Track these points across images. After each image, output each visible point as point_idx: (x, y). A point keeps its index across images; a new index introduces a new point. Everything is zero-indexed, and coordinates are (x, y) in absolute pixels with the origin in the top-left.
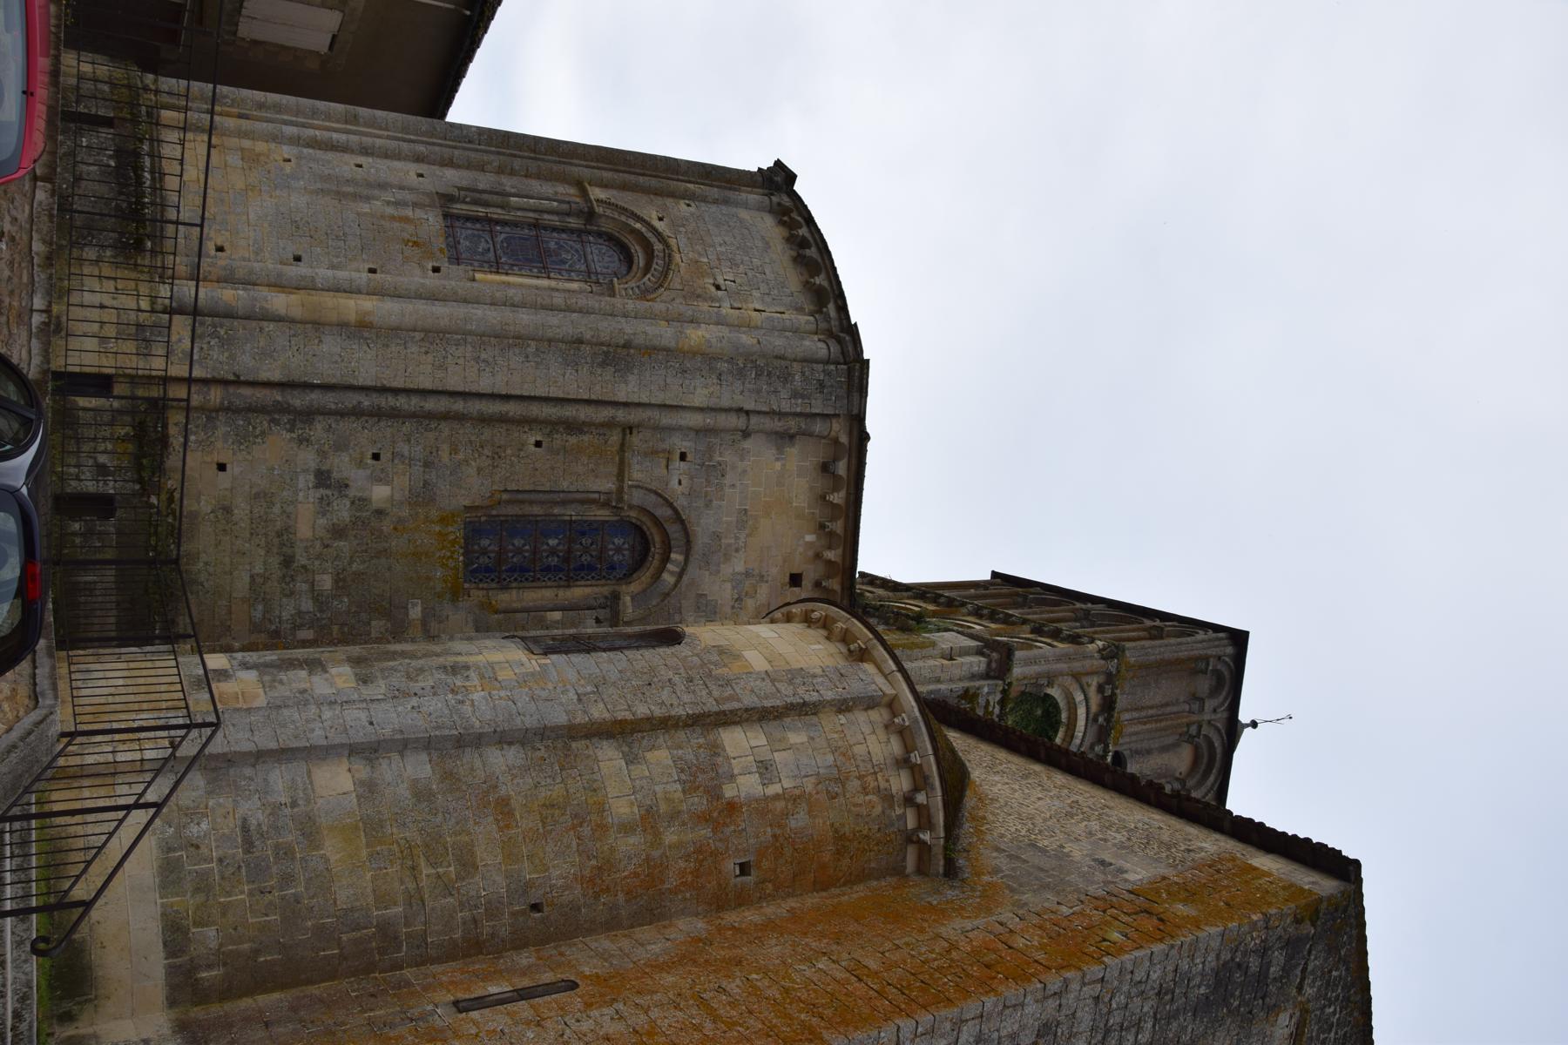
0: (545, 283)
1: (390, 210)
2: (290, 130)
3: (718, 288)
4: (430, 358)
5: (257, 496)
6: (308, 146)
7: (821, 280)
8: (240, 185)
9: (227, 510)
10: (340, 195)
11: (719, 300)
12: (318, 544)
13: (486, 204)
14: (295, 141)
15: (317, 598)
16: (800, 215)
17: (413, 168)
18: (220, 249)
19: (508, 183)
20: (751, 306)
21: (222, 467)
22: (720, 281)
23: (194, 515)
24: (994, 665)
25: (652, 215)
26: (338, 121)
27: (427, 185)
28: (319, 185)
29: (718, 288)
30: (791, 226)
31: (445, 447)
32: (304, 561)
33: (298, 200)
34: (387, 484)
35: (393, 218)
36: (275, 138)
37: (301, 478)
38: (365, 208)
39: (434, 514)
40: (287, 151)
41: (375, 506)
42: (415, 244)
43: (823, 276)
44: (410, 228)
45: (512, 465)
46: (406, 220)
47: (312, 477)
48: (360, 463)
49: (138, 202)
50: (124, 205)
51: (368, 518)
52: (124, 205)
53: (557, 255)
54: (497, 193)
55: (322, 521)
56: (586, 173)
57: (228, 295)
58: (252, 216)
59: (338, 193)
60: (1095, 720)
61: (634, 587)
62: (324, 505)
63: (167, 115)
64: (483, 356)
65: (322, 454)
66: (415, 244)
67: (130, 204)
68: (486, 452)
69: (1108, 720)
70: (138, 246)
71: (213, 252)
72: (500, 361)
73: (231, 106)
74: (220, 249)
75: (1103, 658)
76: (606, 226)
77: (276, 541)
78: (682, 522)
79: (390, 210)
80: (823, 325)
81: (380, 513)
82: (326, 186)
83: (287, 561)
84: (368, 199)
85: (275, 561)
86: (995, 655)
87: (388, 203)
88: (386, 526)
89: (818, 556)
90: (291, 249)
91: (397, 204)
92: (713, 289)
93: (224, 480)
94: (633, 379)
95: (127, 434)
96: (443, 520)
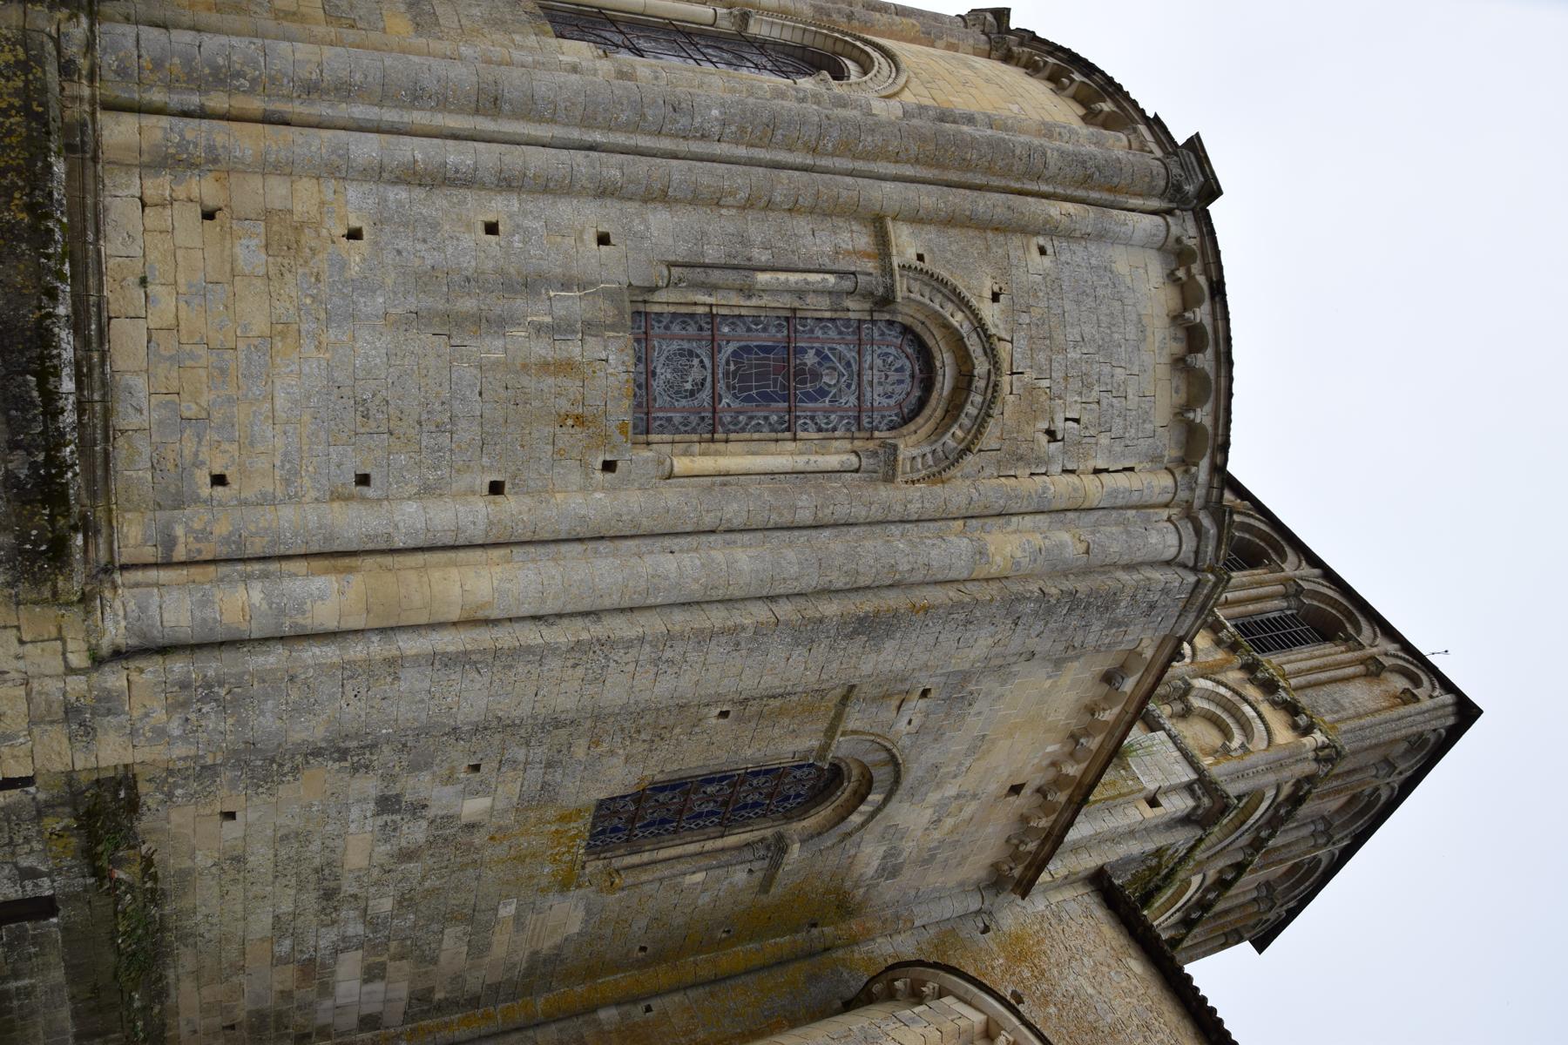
0: (781, 458)
1: (541, 349)
2: (367, 148)
3: (1051, 434)
4: (580, 671)
5: (284, 838)
6: (397, 181)
7: (1203, 416)
8: (260, 325)
9: (239, 860)
10: (451, 324)
11: (1048, 461)
12: (375, 873)
13: (712, 288)
14: (377, 174)
15: (372, 923)
16: (1206, 271)
17: (592, 215)
18: (219, 480)
19: (760, 234)
20: (1091, 464)
21: (230, 816)
22: (1059, 425)
23: (185, 876)
24: (1200, 812)
25: (977, 287)
26: (461, 110)
27: (614, 268)
28: (412, 303)
29: (1051, 434)
30: (1188, 298)
31: (583, 742)
32: (352, 891)
33: (371, 347)
34: (487, 795)
35: (545, 367)
36: (337, 171)
37: (355, 813)
38: (493, 348)
39: (551, 813)
40: (356, 204)
41: (464, 821)
42: (580, 420)
43: (1208, 407)
44: (572, 385)
45: (679, 743)
46: (566, 367)
47: (372, 806)
48: (450, 779)
49: (50, 461)
50: (23, 473)
51: (453, 837)
52: (23, 473)
53: (816, 376)
54: (735, 268)
55: (384, 848)
56: (887, 194)
57: (240, 602)
58: (281, 401)
59: (447, 316)
60: (1280, 805)
61: (811, 822)
62: (389, 832)
63: (118, 131)
64: (668, 654)
65: (389, 777)
66: (580, 420)
67: (34, 466)
68: (643, 736)
69: (1289, 813)
70: (58, 551)
71: (206, 490)
72: (692, 656)
73: (251, 91)
74: (219, 480)
75: (1317, 760)
76: (905, 313)
77: (313, 878)
78: (897, 764)
79: (541, 349)
80: (1183, 495)
81: (471, 827)
82: (427, 302)
83: (329, 895)
84: (500, 324)
85: (310, 899)
86: (1206, 801)
87: (539, 329)
88: (478, 839)
89: (1054, 764)
90: (355, 463)
91: (557, 330)
92: (1044, 438)
93: (232, 830)
94: (890, 646)
95: (65, 829)
96: (563, 819)
